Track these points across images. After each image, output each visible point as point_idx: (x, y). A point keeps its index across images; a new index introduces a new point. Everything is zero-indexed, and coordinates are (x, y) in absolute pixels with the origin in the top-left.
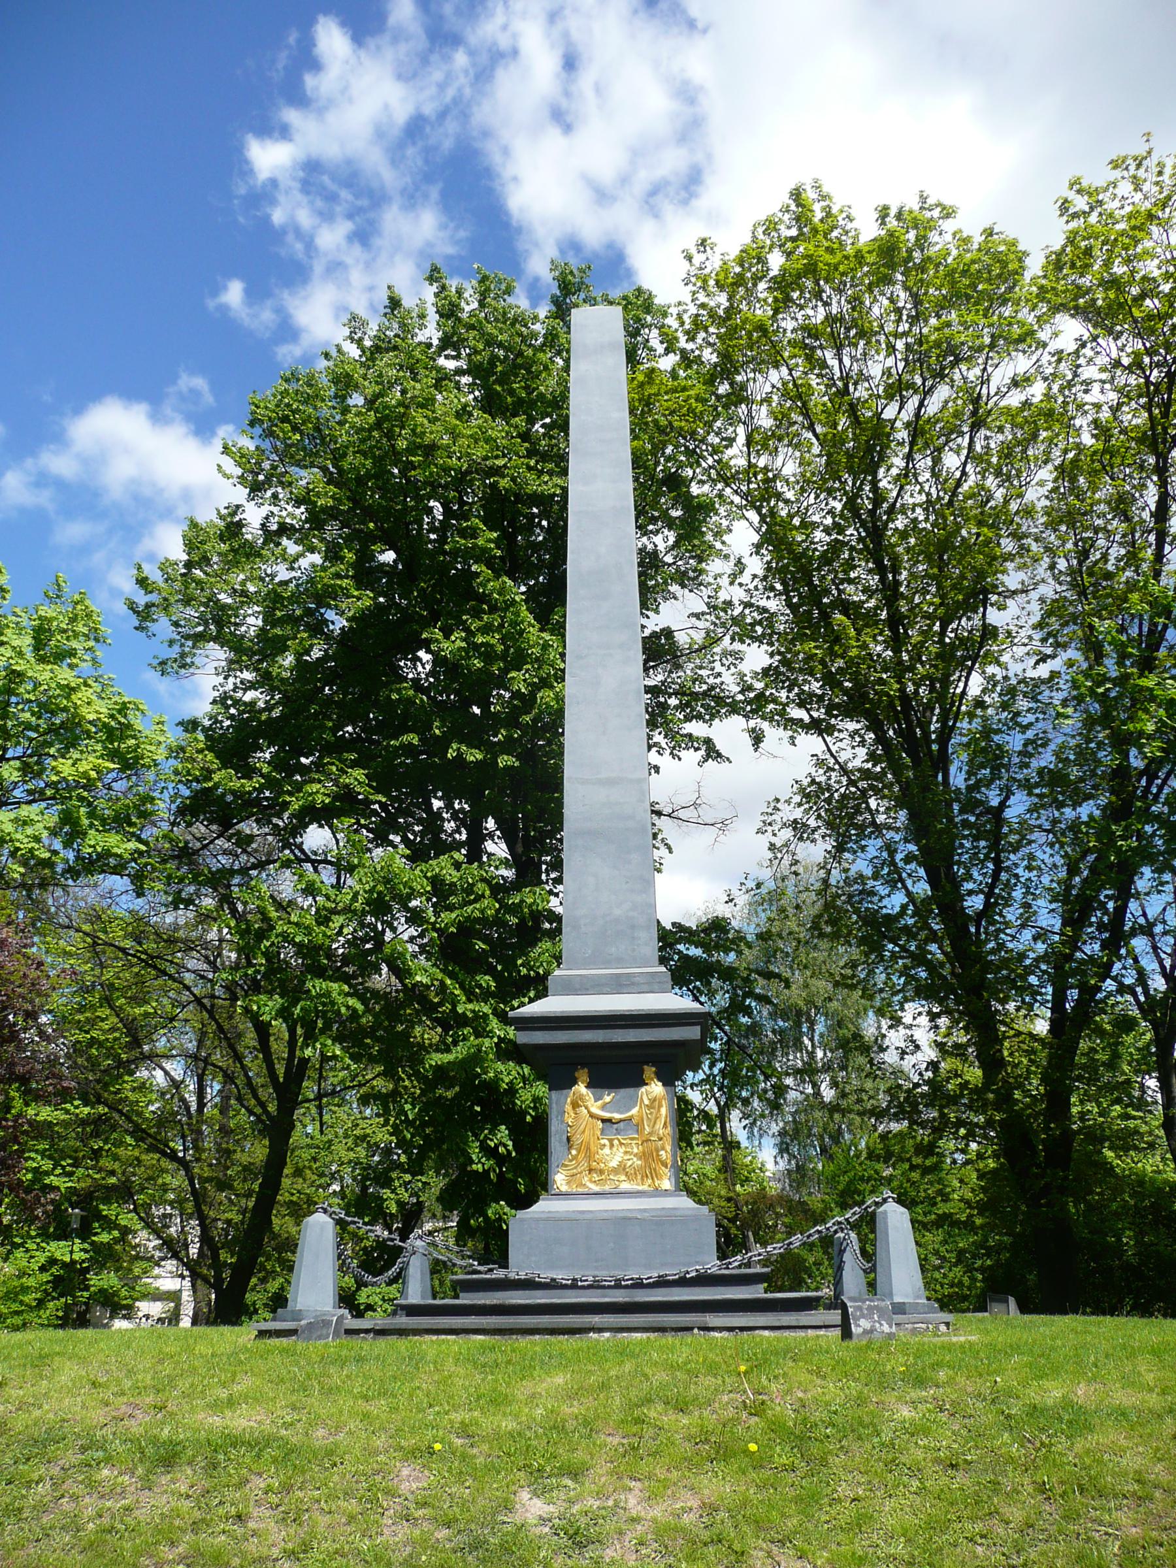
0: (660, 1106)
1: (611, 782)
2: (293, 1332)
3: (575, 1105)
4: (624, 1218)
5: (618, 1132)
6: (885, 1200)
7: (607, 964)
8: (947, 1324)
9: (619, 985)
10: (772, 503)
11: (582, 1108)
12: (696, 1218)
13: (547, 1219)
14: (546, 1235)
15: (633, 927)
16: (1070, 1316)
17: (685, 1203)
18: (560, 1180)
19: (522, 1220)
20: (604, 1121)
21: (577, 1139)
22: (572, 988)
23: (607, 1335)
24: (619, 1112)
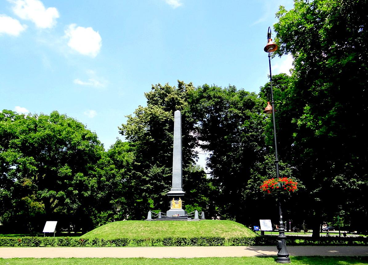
9: (177, 190)
11: (173, 202)
22: (173, 190)
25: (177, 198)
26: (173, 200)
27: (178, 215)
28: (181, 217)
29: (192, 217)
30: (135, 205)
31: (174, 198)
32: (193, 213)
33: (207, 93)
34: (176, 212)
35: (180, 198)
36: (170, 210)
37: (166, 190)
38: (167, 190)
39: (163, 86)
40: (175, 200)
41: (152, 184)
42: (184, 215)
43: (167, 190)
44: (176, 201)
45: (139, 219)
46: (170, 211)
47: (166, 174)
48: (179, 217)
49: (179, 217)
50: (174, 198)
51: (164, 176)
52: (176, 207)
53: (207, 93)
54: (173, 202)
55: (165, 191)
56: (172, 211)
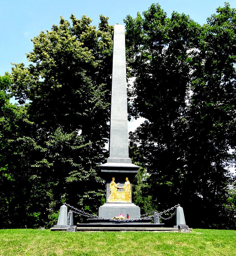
0: (129, 186)
1: (119, 120)
2: (66, 230)
3: (112, 185)
4: (122, 208)
5: (120, 190)
6: (178, 206)
7: (119, 157)
8: (191, 230)
9: (122, 161)
10: (96, 142)
11: (113, 186)
12: (137, 208)
13: (106, 208)
14: (104, 212)
15: (124, 150)
16: (222, 230)
17: (133, 205)
18: (108, 200)
19: (102, 208)
20: (118, 188)
21: (112, 192)
22: (111, 161)
23: (125, 231)
24: (121, 186)
25: (120, 179)
26: (113, 182)
27: (128, 217)
28: (135, 221)
29: (170, 222)
30: (231, 44)
31: (114, 179)
32: (172, 211)
33: (8, 175)
34: (122, 208)
35: (127, 179)
36: (105, 205)
37: (74, 173)
38: (76, 172)
39: (87, 18)
40: (116, 182)
41: (50, 160)
42: (138, 219)
43: (76, 172)
44: (118, 184)
45: (31, 224)
46: (108, 208)
47: (74, 145)
48: (130, 222)
49: (130, 222)
50: (114, 179)
51: (73, 148)
52: (119, 200)
53: (8, 175)
54: (113, 186)
55: (72, 174)
56: (112, 208)
